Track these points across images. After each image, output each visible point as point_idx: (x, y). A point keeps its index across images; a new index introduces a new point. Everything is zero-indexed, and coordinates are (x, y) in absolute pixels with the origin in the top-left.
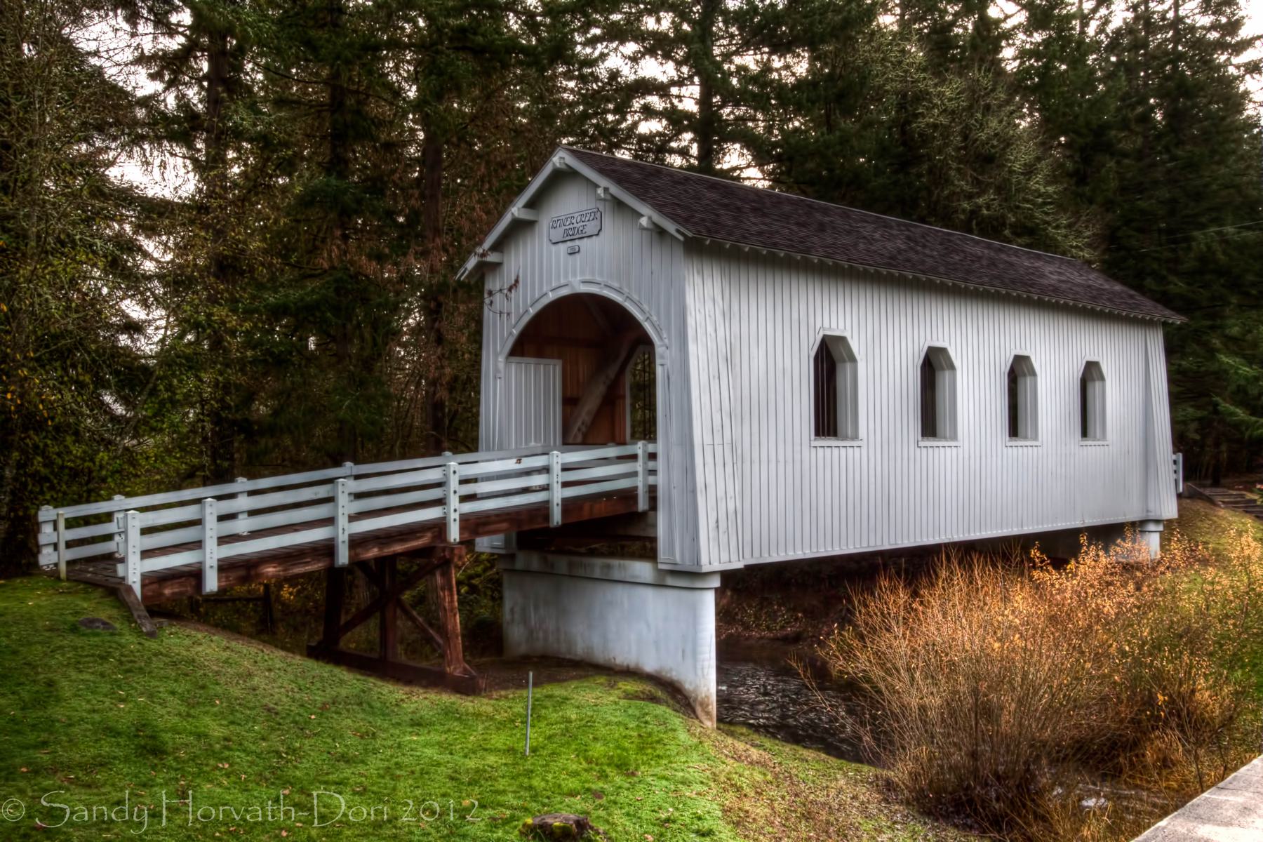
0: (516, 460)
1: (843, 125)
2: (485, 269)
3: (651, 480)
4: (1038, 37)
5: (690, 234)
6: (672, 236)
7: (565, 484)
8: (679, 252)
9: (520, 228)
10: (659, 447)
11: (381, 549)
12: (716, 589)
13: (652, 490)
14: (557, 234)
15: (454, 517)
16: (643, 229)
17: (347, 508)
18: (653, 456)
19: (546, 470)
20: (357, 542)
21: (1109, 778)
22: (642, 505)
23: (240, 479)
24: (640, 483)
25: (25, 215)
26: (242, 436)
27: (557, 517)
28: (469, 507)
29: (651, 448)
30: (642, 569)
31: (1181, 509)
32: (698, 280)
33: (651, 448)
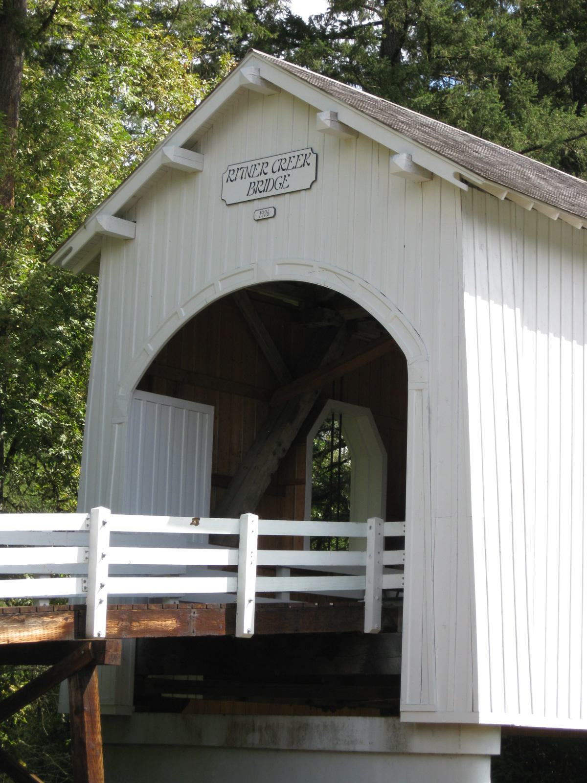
1: (75, 477)
3: (391, 581)
4: (80, 347)
7: (264, 571)
8: (452, 208)
10: (410, 528)
12: (494, 758)
13: (392, 603)
14: (239, 190)
16: (401, 174)
18: (395, 543)
19: (231, 542)
20: (119, 607)
21: (561, 45)
22: (371, 623)
24: (371, 590)
25: (474, 113)
27: (247, 625)
29: (392, 529)
30: (363, 730)
32: (480, 257)
33: (392, 529)
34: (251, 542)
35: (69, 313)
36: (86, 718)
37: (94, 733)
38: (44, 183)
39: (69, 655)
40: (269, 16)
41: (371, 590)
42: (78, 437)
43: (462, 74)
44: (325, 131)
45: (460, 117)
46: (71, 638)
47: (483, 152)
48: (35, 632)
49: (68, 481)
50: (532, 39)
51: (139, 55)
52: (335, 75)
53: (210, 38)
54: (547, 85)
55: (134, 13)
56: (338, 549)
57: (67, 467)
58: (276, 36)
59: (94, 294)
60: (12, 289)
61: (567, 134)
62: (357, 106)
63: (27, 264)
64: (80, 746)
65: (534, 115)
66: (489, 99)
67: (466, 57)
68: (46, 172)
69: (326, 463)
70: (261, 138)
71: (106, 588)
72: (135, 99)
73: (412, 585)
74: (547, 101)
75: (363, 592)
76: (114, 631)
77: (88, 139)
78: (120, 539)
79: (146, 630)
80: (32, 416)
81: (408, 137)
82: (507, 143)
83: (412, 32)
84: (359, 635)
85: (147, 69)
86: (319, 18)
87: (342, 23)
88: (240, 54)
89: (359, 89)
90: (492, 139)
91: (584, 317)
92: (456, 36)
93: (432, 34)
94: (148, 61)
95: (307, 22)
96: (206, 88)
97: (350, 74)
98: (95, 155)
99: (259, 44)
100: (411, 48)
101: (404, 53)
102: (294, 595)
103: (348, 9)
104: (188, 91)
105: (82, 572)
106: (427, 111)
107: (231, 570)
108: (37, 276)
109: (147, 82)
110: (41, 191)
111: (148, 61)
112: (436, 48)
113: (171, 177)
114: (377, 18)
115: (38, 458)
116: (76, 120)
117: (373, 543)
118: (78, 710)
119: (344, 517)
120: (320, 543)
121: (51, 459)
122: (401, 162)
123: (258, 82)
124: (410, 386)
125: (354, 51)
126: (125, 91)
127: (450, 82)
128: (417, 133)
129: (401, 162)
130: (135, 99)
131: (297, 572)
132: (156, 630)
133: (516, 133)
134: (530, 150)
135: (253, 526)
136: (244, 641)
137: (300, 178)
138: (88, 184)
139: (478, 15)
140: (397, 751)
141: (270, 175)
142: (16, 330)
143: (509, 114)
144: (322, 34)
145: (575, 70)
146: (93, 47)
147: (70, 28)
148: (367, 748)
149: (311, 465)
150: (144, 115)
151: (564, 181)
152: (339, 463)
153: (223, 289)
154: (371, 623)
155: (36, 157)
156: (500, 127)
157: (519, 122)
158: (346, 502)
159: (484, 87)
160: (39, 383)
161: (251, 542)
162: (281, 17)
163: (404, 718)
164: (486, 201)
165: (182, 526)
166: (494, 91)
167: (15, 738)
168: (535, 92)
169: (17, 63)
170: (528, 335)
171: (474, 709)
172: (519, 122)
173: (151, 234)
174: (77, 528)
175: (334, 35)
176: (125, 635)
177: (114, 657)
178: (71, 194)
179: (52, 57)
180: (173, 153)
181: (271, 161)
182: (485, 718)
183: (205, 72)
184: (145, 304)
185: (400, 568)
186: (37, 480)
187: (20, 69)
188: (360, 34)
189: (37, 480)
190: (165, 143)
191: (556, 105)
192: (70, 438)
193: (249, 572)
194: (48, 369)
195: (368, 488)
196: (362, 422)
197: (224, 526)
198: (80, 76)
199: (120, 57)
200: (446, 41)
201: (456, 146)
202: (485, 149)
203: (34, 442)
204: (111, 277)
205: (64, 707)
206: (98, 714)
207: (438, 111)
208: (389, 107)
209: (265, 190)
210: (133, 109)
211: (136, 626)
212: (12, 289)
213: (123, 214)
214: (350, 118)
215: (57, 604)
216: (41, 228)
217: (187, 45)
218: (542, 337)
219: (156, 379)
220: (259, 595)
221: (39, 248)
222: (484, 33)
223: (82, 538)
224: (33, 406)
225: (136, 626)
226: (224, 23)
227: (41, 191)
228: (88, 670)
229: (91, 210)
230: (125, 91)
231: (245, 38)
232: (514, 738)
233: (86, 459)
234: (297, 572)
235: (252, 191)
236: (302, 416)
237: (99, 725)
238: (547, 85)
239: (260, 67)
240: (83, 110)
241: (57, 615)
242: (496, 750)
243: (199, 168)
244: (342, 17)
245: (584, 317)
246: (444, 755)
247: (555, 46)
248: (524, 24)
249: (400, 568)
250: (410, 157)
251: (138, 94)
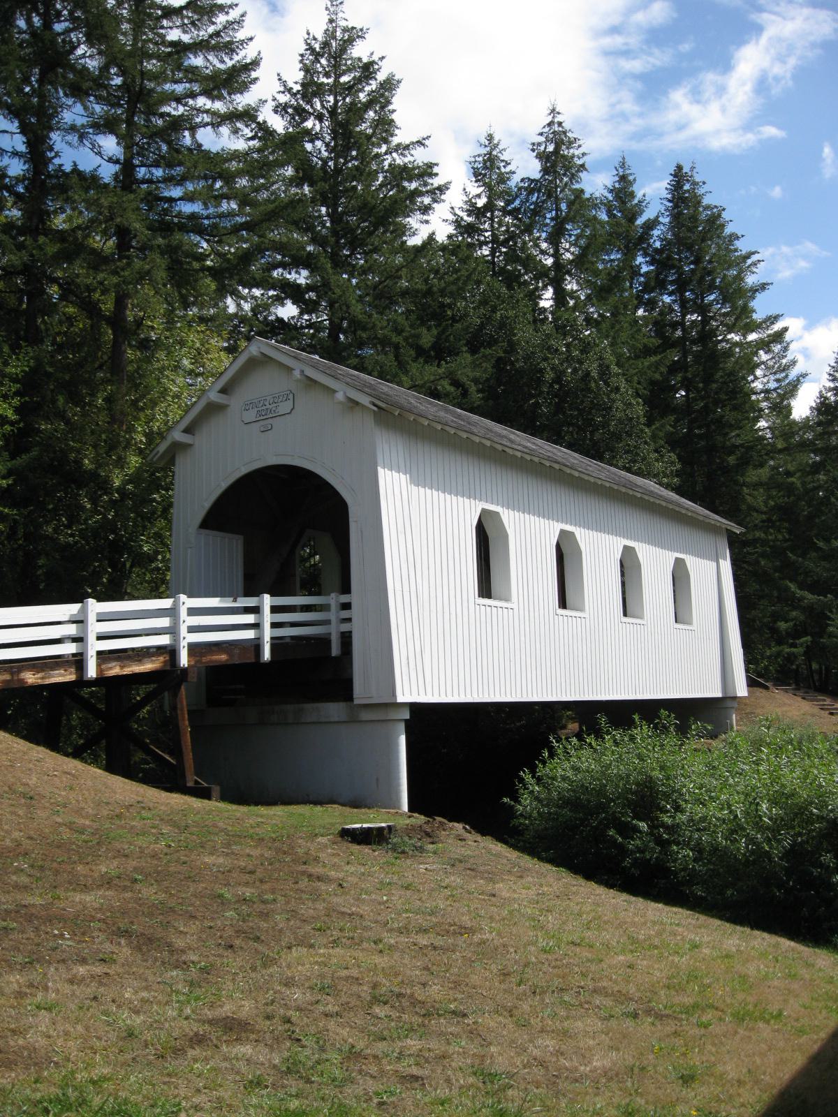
0: (191, 621)
3: (345, 627)
6: (363, 406)
8: (369, 421)
10: (355, 598)
11: (122, 667)
12: (406, 721)
13: (346, 639)
14: (251, 415)
15: (268, 633)
16: (341, 403)
18: (347, 606)
19: (256, 610)
20: (194, 648)
22: (335, 651)
24: (334, 631)
27: (267, 655)
28: (280, 632)
29: (344, 599)
30: (334, 710)
31: (749, 692)
32: (386, 448)
33: (344, 599)
35: (158, 488)
36: (179, 712)
37: (183, 720)
38: (142, 415)
39: (168, 676)
40: (265, 318)
41: (334, 631)
42: (168, 556)
43: (374, 346)
44: (298, 381)
45: (373, 371)
46: (168, 668)
47: (386, 389)
48: (148, 666)
49: (164, 581)
50: (412, 326)
51: (193, 341)
52: (303, 350)
53: (232, 331)
54: (420, 352)
55: (188, 319)
56: (316, 611)
57: (163, 573)
58: (268, 329)
59: (173, 476)
60: (126, 475)
61: (432, 378)
62: (315, 366)
63: (134, 461)
64: (177, 727)
65: (414, 368)
66: (389, 361)
67: (376, 337)
68: (142, 409)
69: (307, 564)
70: (262, 385)
71: (187, 638)
72: (191, 367)
74: (421, 360)
75: (330, 634)
76: (192, 663)
77: (166, 390)
78: (193, 612)
79: (211, 661)
80: (141, 546)
81: (345, 383)
82: (400, 384)
83: (345, 324)
84: (329, 658)
85: (198, 350)
86: (293, 318)
87: (307, 320)
88: (249, 339)
89: (317, 357)
90: (391, 382)
92: (370, 326)
93: (356, 325)
94: (198, 345)
95: (286, 320)
96: (231, 359)
97: (311, 349)
98: (170, 399)
99: (260, 334)
100: (344, 334)
101: (341, 336)
102: (292, 638)
103: (309, 313)
104: (222, 361)
105: (173, 631)
106: (355, 368)
107: (256, 626)
108: (140, 467)
109: (197, 357)
110: (140, 420)
111: (198, 345)
112: (359, 332)
113: (213, 409)
114: (325, 317)
115: (147, 570)
116: (159, 379)
118: (174, 708)
119: (319, 594)
121: (153, 570)
122: (340, 396)
123: (259, 355)
124: (350, 520)
125: (313, 335)
126: (186, 362)
127: (369, 351)
128: (348, 380)
129: (340, 396)
130: (191, 367)
131: (293, 625)
132: (216, 661)
133: (404, 378)
134: (413, 387)
135: (267, 601)
137: (285, 407)
138: (167, 415)
139: (382, 314)
140: (353, 720)
141: (268, 406)
142: (130, 499)
143: (400, 368)
144: (295, 327)
145: (436, 342)
146: (166, 338)
147: (153, 328)
148: (337, 719)
149: (299, 570)
150: (198, 375)
151: (431, 403)
152: (315, 565)
153: (244, 470)
154: (335, 651)
155: (137, 401)
156: (395, 376)
157: (406, 372)
158: (320, 585)
159: (386, 354)
160: (144, 527)
162: (272, 318)
163: (356, 702)
164: (389, 417)
165: (228, 603)
166: (391, 357)
167: (142, 726)
168: (414, 355)
169: (123, 348)
170: (415, 488)
171: (394, 695)
172: (406, 372)
173: (204, 442)
174: (168, 606)
175: (302, 327)
176: (198, 665)
177: (193, 678)
178: (158, 421)
179: (145, 345)
180: (214, 396)
181: (268, 398)
182: (400, 699)
183: (231, 350)
184: (204, 477)
185: (349, 620)
186: (146, 581)
187: (125, 352)
188: (317, 327)
189: (146, 581)
190: (208, 390)
191: (426, 362)
192: (164, 557)
193: (267, 626)
194: (149, 520)
195: (331, 577)
197: (251, 602)
198: (161, 355)
199: (182, 343)
200: (364, 329)
201: (371, 386)
202: (386, 387)
203: (143, 560)
204: (183, 468)
205: (166, 707)
206: (185, 709)
207: (361, 368)
208: (333, 366)
209: (266, 416)
210: (191, 373)
211: (204, 660)
212: (126, 475)
213: (188, 430)
214: (311, 373)
215: (160, 649)
216: (141, 441)
217: (220, 335)
218: (422, 490)
219: (206, 524)
220: (272, 638)
221: (141, 452)
222: (385, 324)
223: (172, 612)
224: (142, 540)
225: (204, 660)
226: (240, 323)
227: (140, 420)
229: (169, 429)
230: (186, 362)
231: (252, 330)
232: (415, 708)
233: (173, 569)
234: (293, 625)
237: (186, 716)
238: (420, 352)
239: (259, 346)
240: (162, 373)
241: (159, 656)
242: (407, 717)
243: (190, 442)
244: (306, 317)
246: (379, 721)
247: (424, 330)
248: (407, 319)
249: (349, 620)
250: (345, 393)
251: (192, 364)
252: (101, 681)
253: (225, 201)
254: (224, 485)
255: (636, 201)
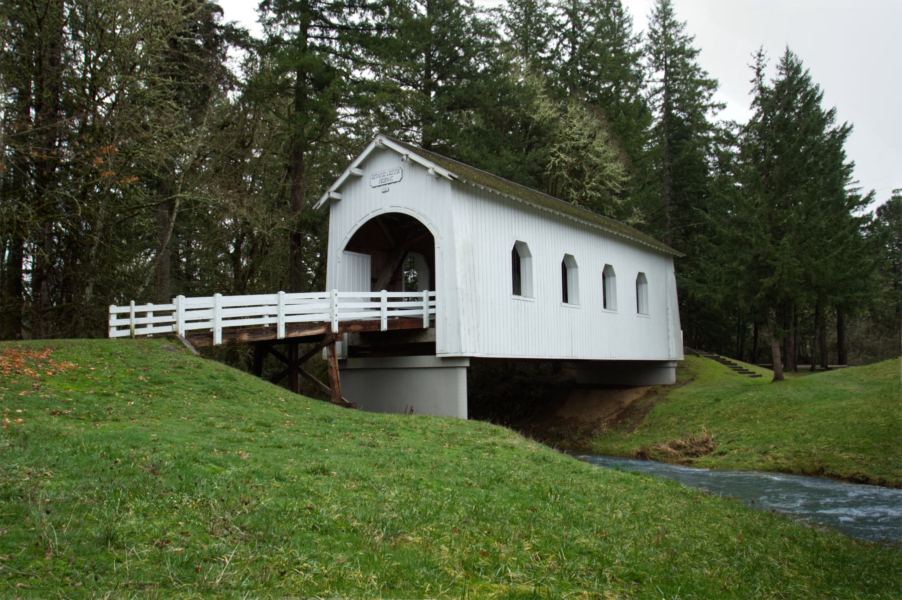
0: (345, 299)
2: (332, 202)
3: (432, 311)
5: (456, 177)
9: (354, 179)
10: (436, 293)
12: (467, 368)
13: (432, 323)
16: (430, 175)
17: (282, 310)
18: (432, 298)
19: (378, 300)
22: (426, 324)
23: (149, 304)
24: (425, 313)
26: (857, 214)
27: (384, 327)
29: (431, 294)
30: (425, 361)
33: (431, 294)
34: (384, 300)
73: (438, 311)
91: (251, 317)
102: (400, 317)
117: (425, 299)
120: (408, 299)
131: (400, 309)
136: (383, 332)
153: (372, 216)
161: (384, 300)
163: (438, 356)
193: (384, 309)
196: (421, 259)
209: (385, 185)
228: (333, 342)
234: (400, 309)
235: (625, 578)
236: (400, 258)
245: (251, 317)
249: (434, 307)
252: (286, 340)
253: (107, 112)
254: (360, 225)
255: (802, 74)
